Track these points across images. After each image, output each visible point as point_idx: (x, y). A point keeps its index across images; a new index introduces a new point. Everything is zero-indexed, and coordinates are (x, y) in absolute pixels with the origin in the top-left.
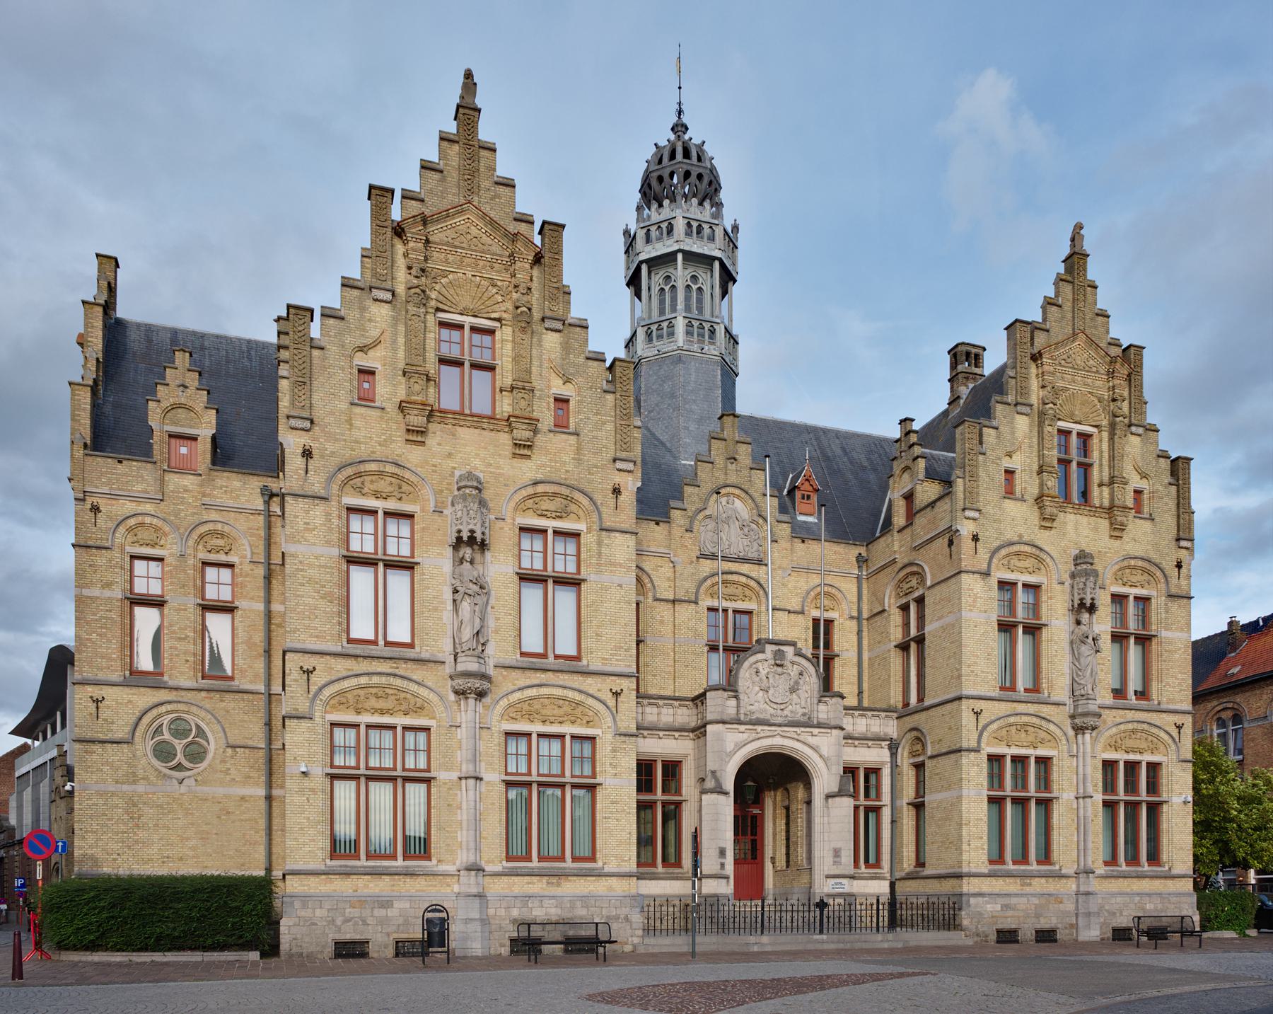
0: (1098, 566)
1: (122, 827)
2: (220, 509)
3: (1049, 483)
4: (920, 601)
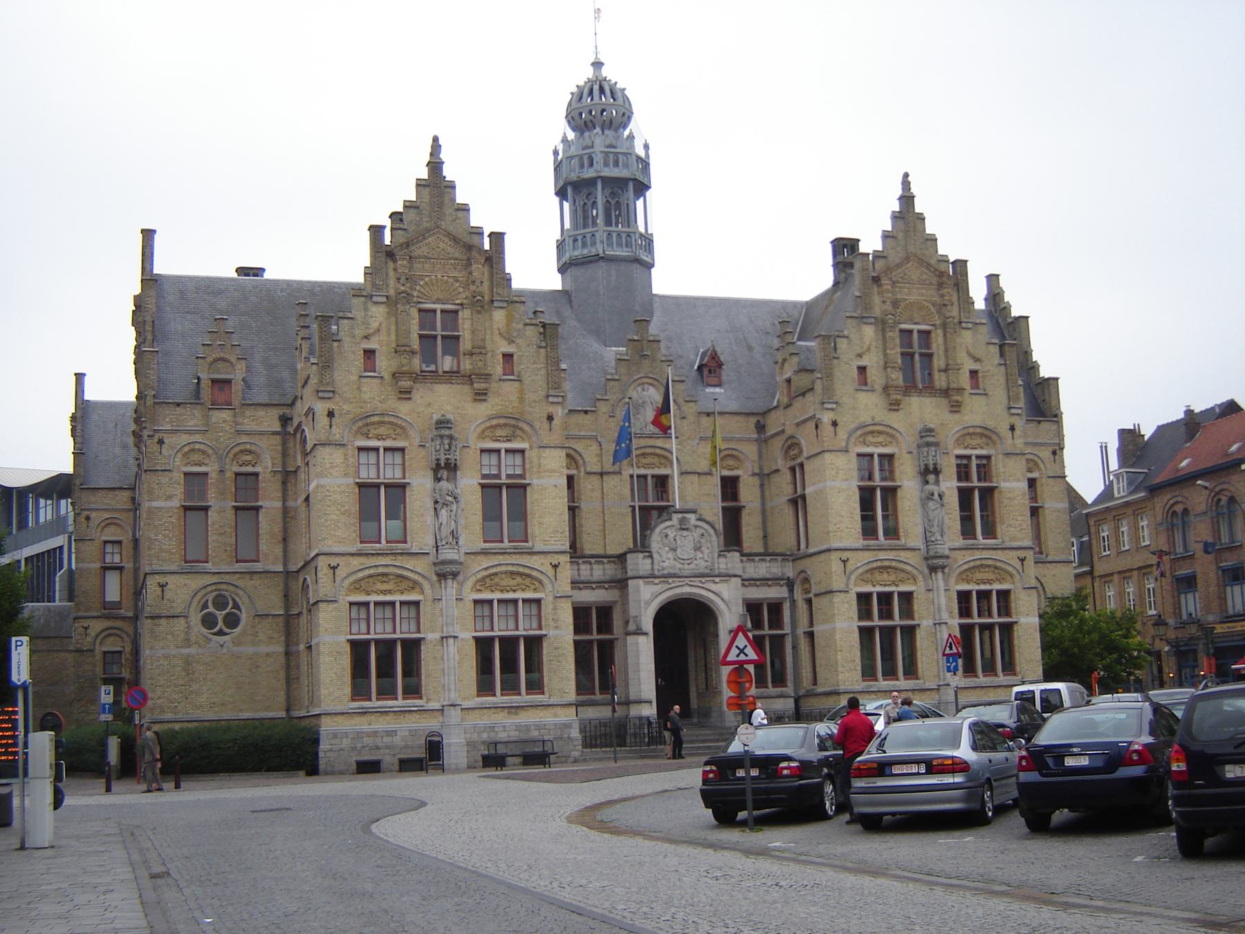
0: (941, 438)
1: (181, 682)
2: (248, 433)
3: (893, 376)
4: (802, 465)
